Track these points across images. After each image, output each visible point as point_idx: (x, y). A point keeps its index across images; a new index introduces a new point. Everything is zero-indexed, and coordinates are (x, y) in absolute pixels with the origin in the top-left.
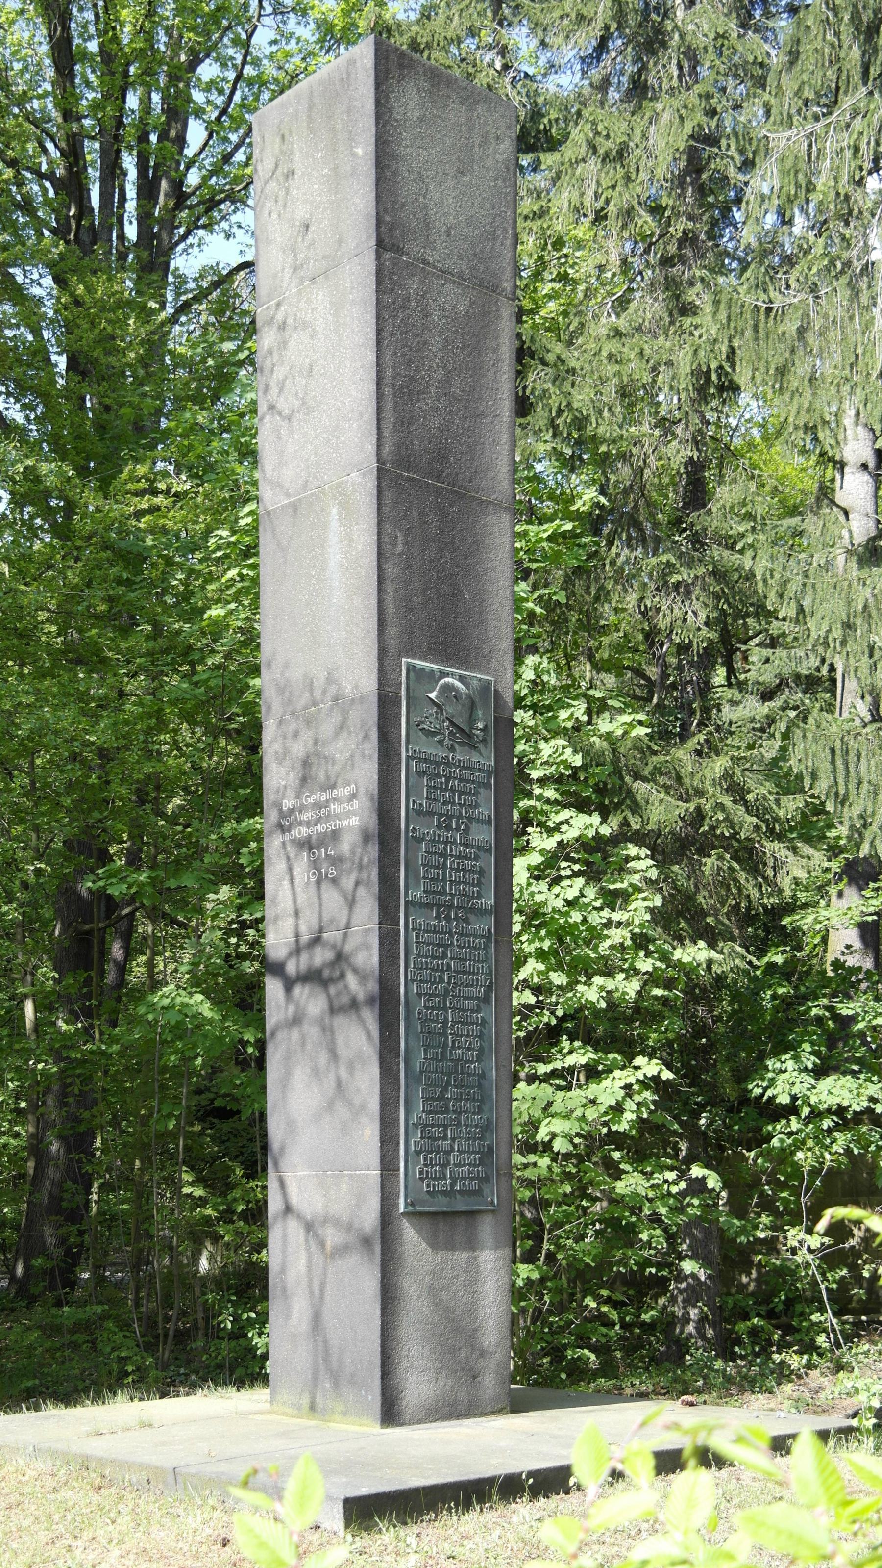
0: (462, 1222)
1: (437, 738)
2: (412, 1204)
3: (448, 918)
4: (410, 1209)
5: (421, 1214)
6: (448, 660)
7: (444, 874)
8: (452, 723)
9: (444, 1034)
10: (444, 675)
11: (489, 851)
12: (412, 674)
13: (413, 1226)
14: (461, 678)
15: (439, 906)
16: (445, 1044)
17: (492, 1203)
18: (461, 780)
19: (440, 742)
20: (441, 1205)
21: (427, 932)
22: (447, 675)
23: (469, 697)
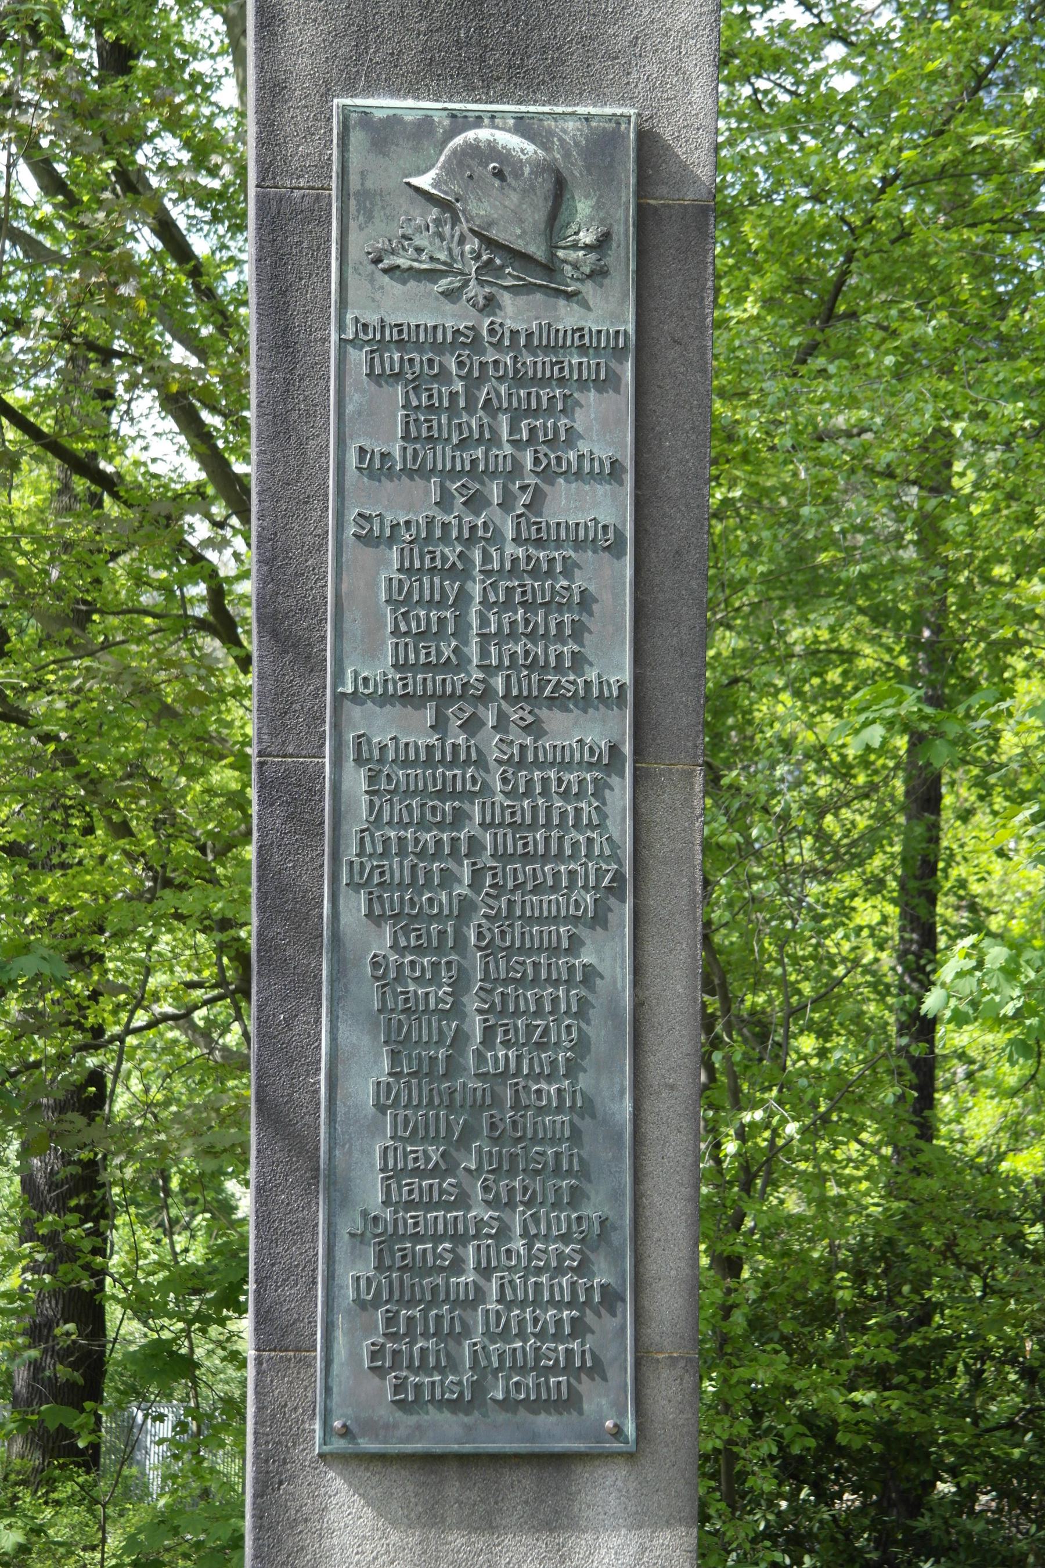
0: (522, 1484)
1: (444, 283)
2: (346, 1432)
3: (472, 725)
4: (339, 1444)
5: (383, 1458)
6: (488, 82)
7: (461, 621)
8: (489, 242)
9: (457, 1010)
10: (460, 122)
11: (615, 549)
12: (357, 137)
13: (356, 1487)
14: (523, 126)
15: (444, 700)
16: (460, 1038)
17: (618, 1432)
18: (519, 380)
19: (450, 295)
20: (445, 1432)
21: (406, 764)
22: (478, 122)
23: (541, 168)
